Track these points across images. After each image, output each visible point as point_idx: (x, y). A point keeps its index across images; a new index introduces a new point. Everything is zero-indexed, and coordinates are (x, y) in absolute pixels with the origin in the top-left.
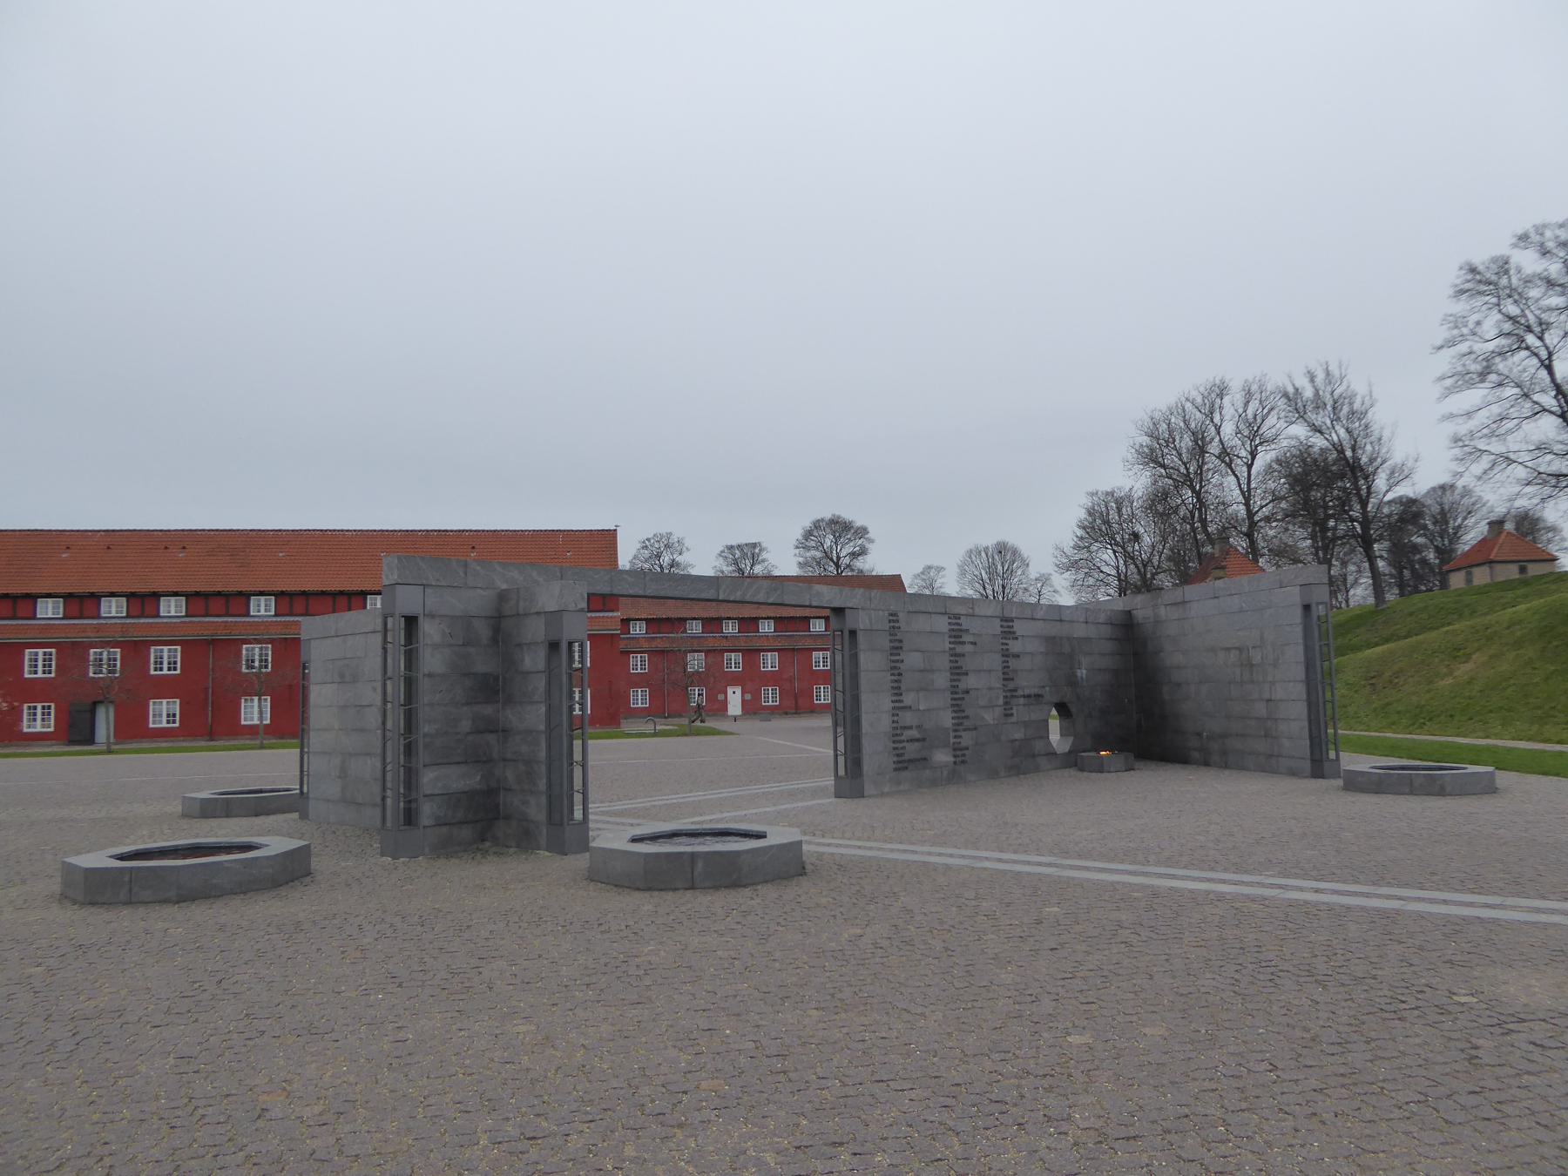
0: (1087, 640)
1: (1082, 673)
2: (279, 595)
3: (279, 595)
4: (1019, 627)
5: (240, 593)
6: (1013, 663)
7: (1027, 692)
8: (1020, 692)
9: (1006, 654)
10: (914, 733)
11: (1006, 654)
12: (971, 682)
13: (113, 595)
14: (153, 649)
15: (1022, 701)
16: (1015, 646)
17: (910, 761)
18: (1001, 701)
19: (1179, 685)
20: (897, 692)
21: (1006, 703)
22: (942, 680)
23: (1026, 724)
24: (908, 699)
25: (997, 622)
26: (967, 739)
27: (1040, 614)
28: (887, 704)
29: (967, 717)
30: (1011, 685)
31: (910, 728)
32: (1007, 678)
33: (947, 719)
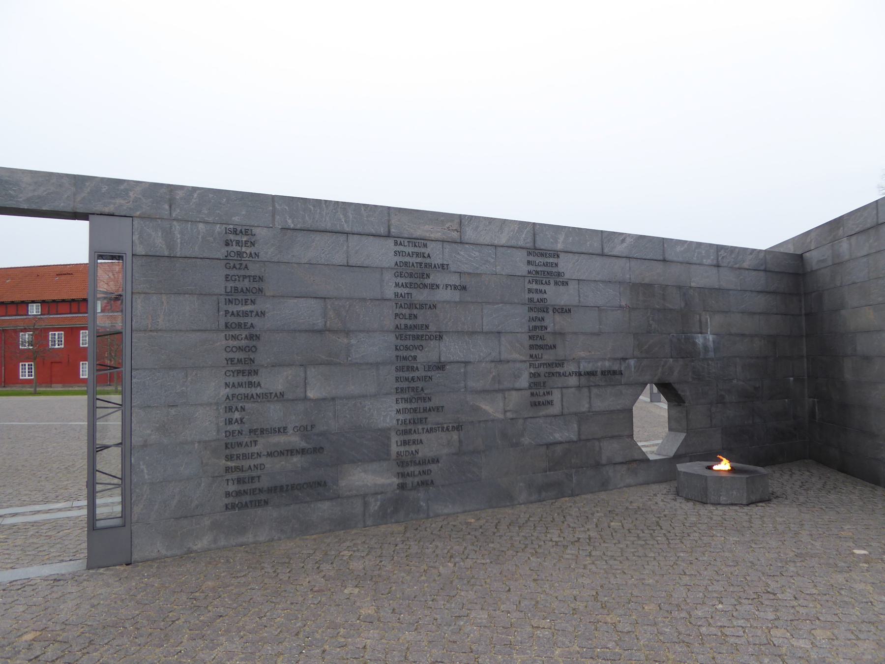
0: (719, 291)
1: (705, 339)
2: (43, 302)
3: (43, 302)
4: (567, 266)
5: (23, 302)
6: (553, 322)
7: (585, 367)
8: (571, 367)
9: (539, 308)
10: (294, 440)
11: (539, 308)
12: (451, 349)
13: (33, 302)
14: (120, 314)
15: (573, 381)
16: (555, 295)
17: (272, 490)
18: (524, 381)
19: (867, 358)
20: (244, 366)
21: (534, 385)
22: (376, 346)
23: (581, 418)
24: (275, 381)
25: (521, 257)
26: (433, 445)
27: (620, 249)
28: (214, 388)
29: (438, 409)
30: (548, 356)
31: (283, 430)
32: (539, 340)
33: (386, 413)
